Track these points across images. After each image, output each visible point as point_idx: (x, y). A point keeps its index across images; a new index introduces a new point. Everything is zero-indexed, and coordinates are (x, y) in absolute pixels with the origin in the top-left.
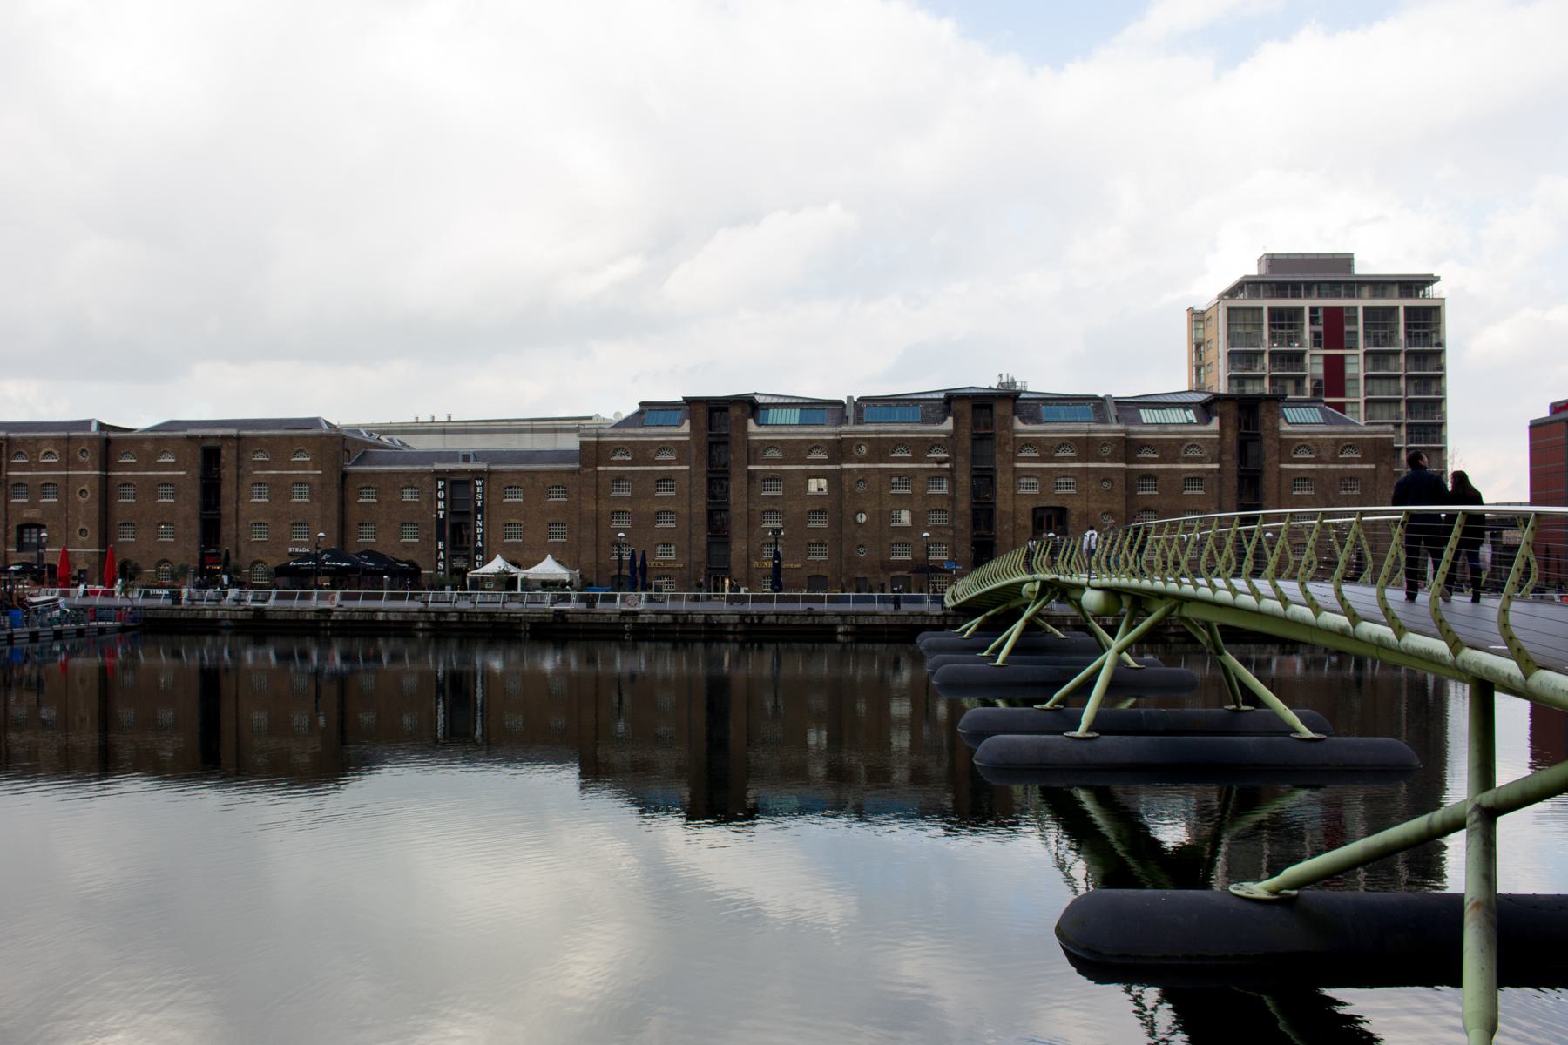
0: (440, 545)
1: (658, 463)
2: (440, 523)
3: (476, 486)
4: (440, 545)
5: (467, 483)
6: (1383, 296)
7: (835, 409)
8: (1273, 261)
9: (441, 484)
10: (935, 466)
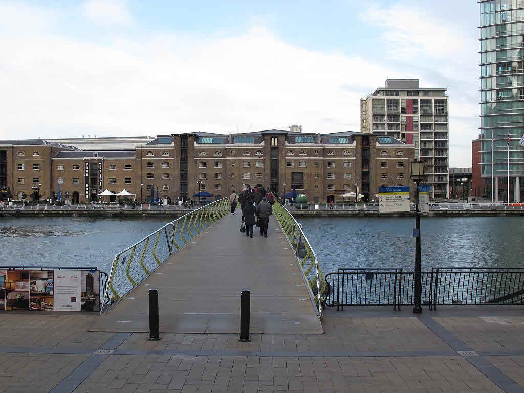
0: (87, 185)
2: (87, 178)
3: (99, 165)
4: (87, 185)
5: (96, 164)
6: (428, 95)
7: (225, 138)
8: (390, 82)
9: (87, 164)
10: (258, 158)
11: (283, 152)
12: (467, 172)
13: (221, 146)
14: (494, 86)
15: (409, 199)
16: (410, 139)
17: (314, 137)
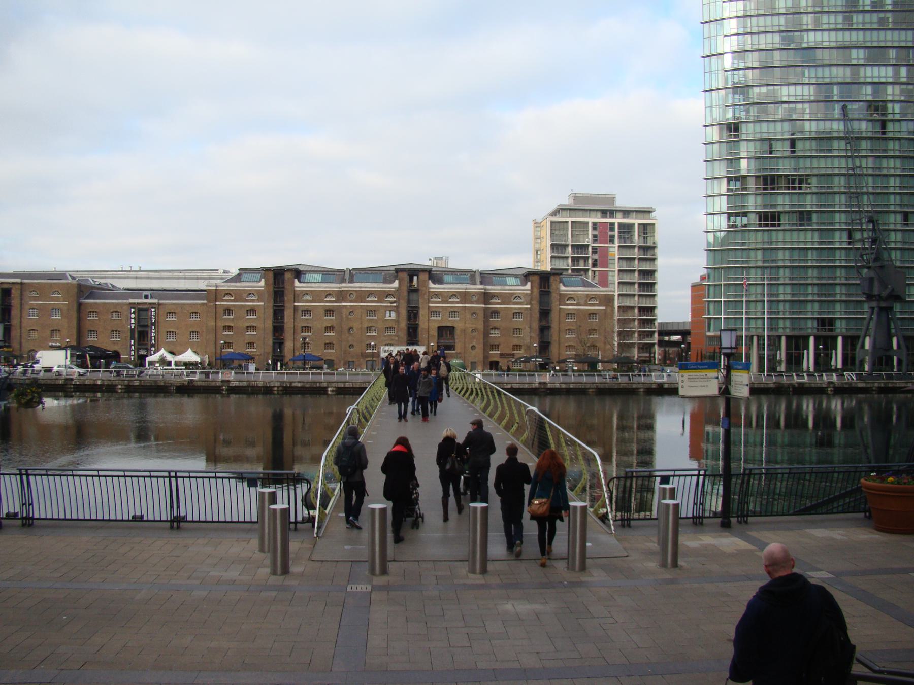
0: (132, 342)
1: (248, 301)
2: (132, 331)
3: (151, 311)
5: (147, 310)
9: (133, 310)
10: (389, 305)
11: (426, 297)
12: (681, 328)
13: (334, 287)
14: (724, 208)
15: (747, 385)
16: (604, 280)
17: (471, 276)
